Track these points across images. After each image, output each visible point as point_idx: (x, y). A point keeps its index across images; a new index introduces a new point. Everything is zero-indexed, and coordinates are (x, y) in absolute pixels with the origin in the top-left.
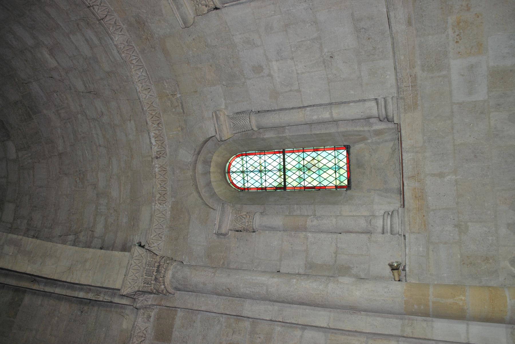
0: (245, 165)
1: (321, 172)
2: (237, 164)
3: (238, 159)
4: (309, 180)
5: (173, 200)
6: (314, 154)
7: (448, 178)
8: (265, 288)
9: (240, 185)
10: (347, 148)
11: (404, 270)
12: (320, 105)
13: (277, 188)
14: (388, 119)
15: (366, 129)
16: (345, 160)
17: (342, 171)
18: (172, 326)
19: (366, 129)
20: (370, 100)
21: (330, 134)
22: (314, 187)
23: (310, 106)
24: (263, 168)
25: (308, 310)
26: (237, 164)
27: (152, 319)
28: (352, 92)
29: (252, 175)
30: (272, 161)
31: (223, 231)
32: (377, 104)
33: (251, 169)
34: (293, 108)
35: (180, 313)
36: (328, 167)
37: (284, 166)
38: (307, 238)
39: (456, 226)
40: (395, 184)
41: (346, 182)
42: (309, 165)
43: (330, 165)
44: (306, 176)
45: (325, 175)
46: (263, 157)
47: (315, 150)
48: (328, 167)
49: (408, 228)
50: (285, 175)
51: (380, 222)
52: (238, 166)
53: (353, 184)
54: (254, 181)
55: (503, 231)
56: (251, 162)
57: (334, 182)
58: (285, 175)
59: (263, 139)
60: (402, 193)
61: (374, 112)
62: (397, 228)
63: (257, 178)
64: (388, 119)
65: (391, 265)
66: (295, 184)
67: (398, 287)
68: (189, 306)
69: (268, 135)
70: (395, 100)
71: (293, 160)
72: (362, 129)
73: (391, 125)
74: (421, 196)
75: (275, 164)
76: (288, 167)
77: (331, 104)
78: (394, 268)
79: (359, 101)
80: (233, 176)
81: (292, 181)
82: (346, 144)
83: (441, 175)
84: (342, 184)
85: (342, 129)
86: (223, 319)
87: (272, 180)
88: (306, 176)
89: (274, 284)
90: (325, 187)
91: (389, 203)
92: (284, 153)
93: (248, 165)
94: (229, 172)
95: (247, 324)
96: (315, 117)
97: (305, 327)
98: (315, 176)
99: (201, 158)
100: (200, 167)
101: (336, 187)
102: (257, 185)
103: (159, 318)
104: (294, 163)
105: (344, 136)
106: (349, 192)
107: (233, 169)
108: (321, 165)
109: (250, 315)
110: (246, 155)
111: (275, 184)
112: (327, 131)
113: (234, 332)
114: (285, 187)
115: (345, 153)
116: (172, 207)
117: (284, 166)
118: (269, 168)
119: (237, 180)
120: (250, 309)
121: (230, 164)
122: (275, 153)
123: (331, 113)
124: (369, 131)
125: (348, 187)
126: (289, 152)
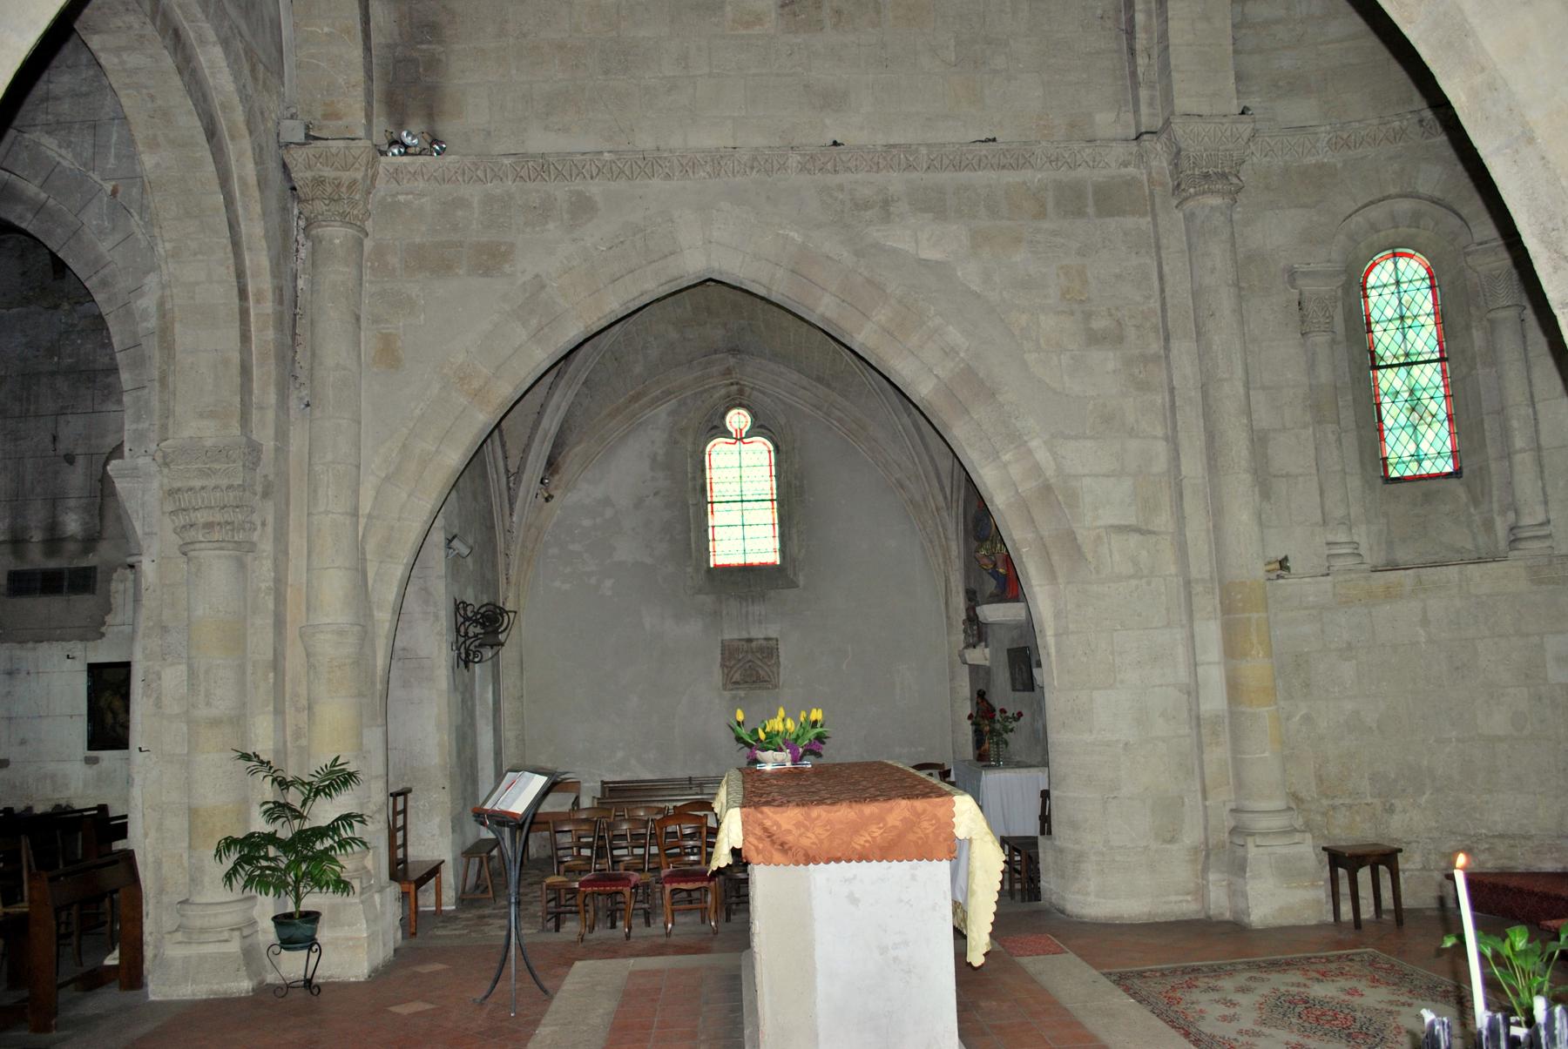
0: (1411, 287)
1: (1410, 430)
2: (1413, 268)
3: (1423, 273)
4: (1394, 411)
5: (1339, 165)
6: (1442, 415)
7: (1421, 632)
8: (1226, 376)
9: (1371, 280)
10: (1457, 473)
11: (1279, 577)
12: (1537, 431)
13: (1373, 353)
14: (1514, 542)
15: (1495, 506)
16: (1434, 471)
17: (1414, 467)
18: (1121, 212)
19: (1495, 506)
20: (1547, 511)
21: (1483, 445)
22: (1380, 420)
23: (1535, 413)
24: (1409, 322)
25: (1199, 441)
26: (1413, 268)
27: (1123, 171)
28: (1561, 484)
29: (1394, 302)
30: (1425, 339)
31: (1299, 282)
32: (1541, 525)
33: (1406, 298)
34: (1530, 382)
35: (1145, 222)
36: (1419, 441)
37: (1417, 363)
38: (1305, 426)
39: (1349, 644)
40: (1402, 555)
41: (1394, 474)
42: (1420, 409)
43: (1424, 446)
44: (1400, 405)
45: (1404, 437)
46: (1431, 321)
47: (1450, 418)
48: (1419, 441)
49: (1341, 578)
50: (1399, 365)
51: (1342, 538)
52: (1409, 275)
53: (1392, 486)
54: (1380, 305)
55: (1349, 706)
56: (1419, 298)
57: (1393, 455)
58: (1399, 365)
59: (1468, 327)
60: (1393, 567)
61: (1527, 520)
62: (1338, 564)
63: (1389, 313)
64: (1514, 542)
65: (1286, 559)
66: (1384, 386)
67: (1260, 571)
68: (1164, 241)
69: (1478, 336)
70: (1549, 551)
71: (1429, 377)
72: (1495, 499)
73: (1503, 544)
74: (1390, 594)
75: (1419, 346)
76: (1415, 370)
77: (1539, 448)
78: (1283, 564)
79: (1545, 494)
80: (1389, 265)
81: (1388, 380)
82: (1466, 472)
83: (1425, 622)
84: (1390, 469)
85: (1494, 466)
86: (1155, 304)
87: (1386, 341)
88: (1400, 405)
89: (1231, 392)
90: (1383, 439)
91: (1371, 549)
92: (1441, 360)
93: (1412, 294)
94: (1395, 255)
95: (1155, 347)
96: (1515, 424)
97: (1173, 442)
98: (1402, 420)
99: (1425, 206)
100: (1405, 205)
101: (1385, 459)
102: (1375, 315)
103: (1131, 183)
104: (1423, 382)
105: (1481, 469)
106: (1380, 481)
107: (1402, 262)
108: (1422, 428)
109: (1174, 352)
110: (1432, 287)
111: (1380, 350)
112: (1488, 441)
113: (1137, 327)
114: (1376, 368)
115: (1449, 469)
116: (1323, 165)
117: (1417, 363)
118: (1411, 334)
119: (1382, 274)
120: (1183, 349)
121: (1411, 256)
122: (1440, 343)
123: (1522, 450)
124: (1491, 510)
125: (1388, 480)
126: (1444, 371)
